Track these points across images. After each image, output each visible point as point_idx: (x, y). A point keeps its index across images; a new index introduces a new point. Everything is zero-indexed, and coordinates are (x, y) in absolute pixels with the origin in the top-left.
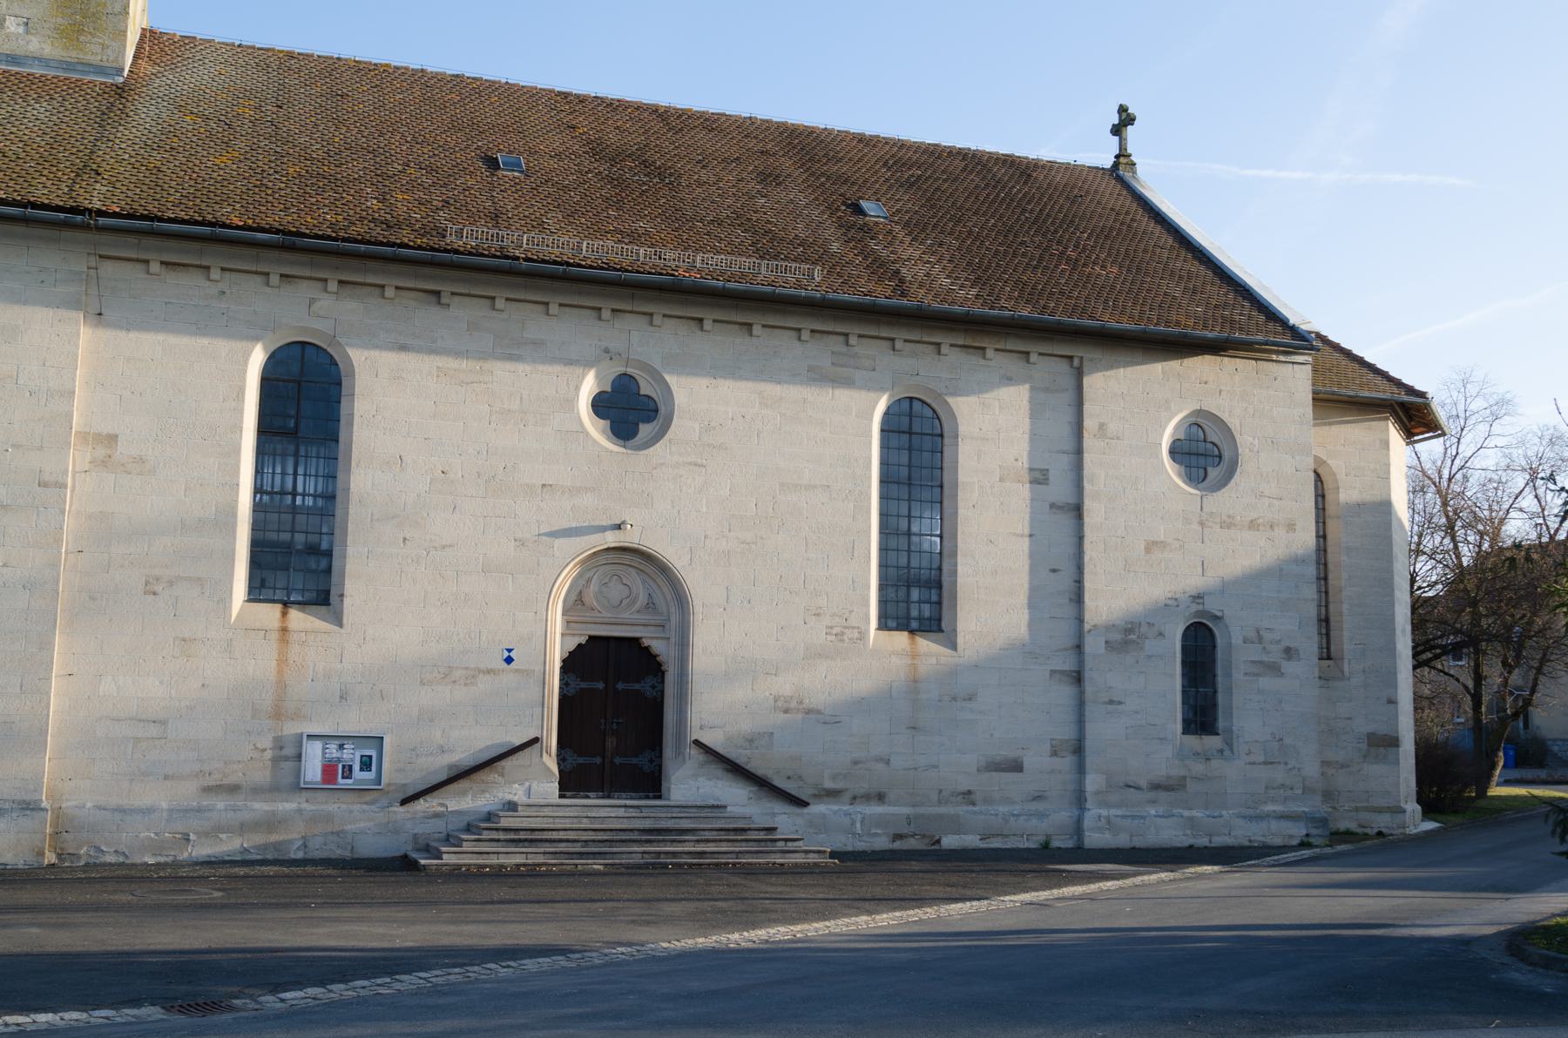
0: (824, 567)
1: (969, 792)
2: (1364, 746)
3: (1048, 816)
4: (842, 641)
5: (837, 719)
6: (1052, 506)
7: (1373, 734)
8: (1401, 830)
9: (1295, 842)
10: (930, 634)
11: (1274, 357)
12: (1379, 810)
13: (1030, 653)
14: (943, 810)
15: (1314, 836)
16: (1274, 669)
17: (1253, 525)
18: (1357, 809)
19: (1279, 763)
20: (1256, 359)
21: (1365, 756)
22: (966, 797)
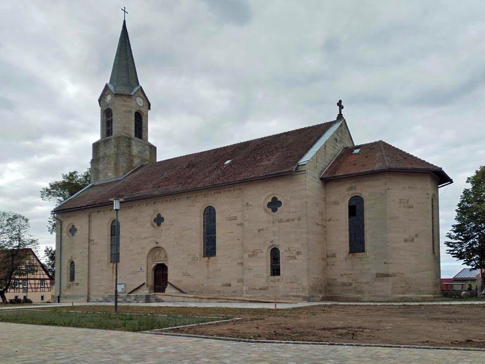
1: (219, 291)
6: (238, 225)
16: (294, 258)
17: (288, 221)
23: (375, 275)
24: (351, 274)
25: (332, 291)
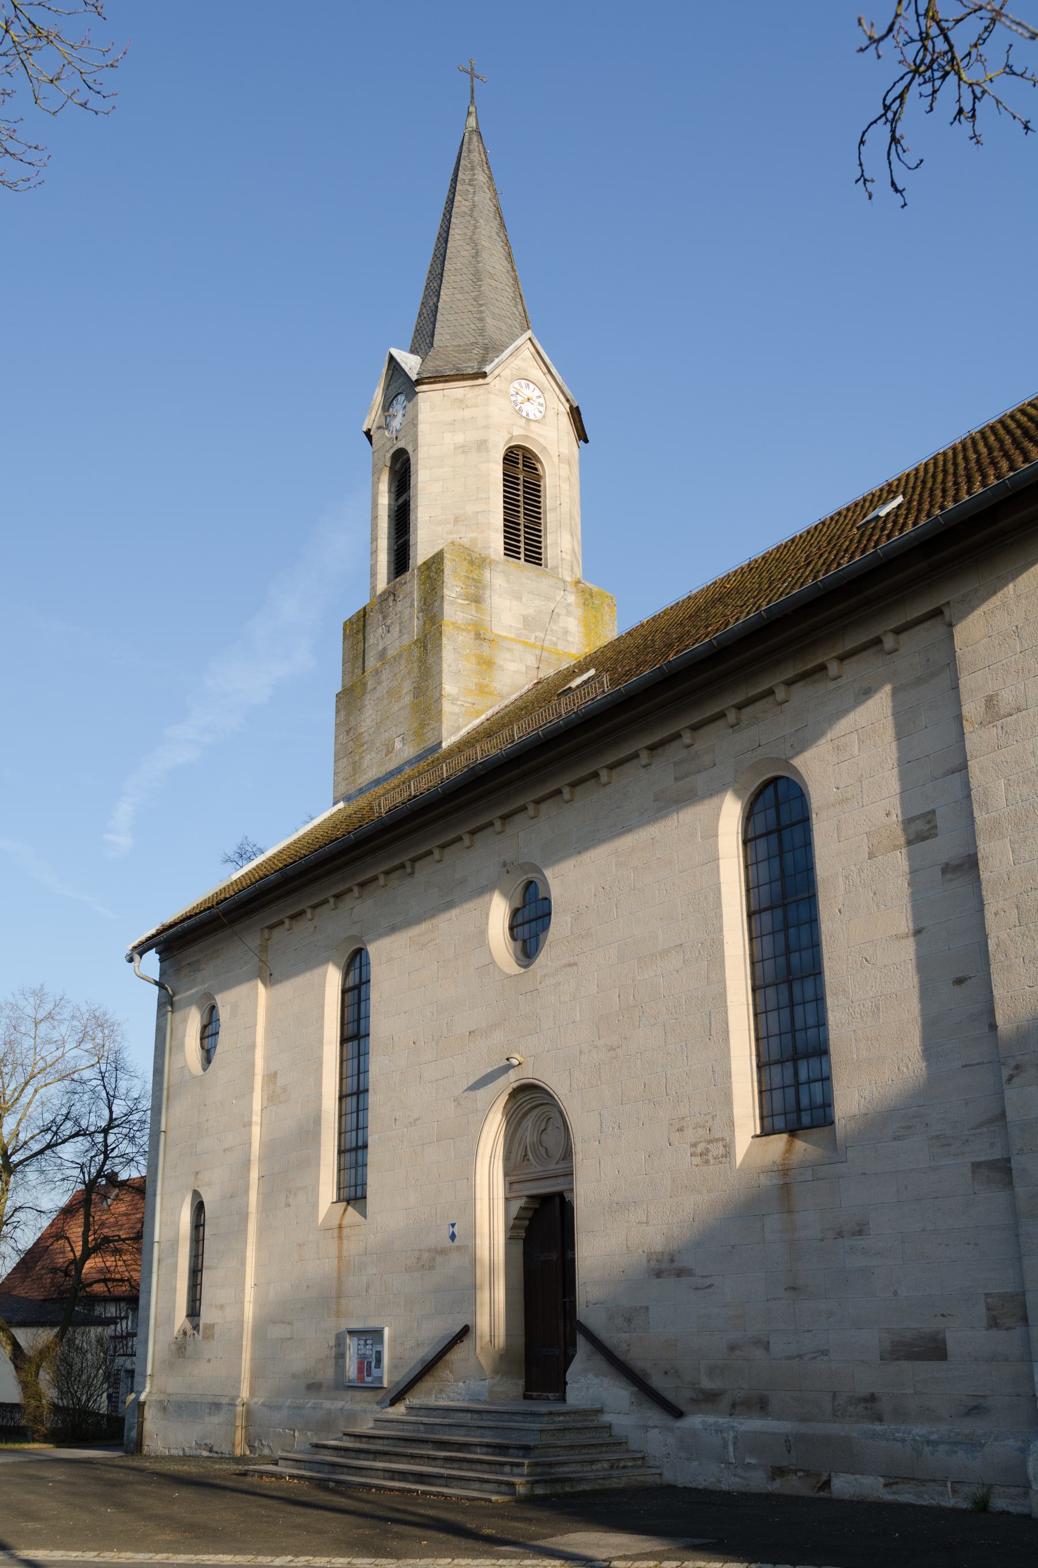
0: (683, 1059)
1: (872, 1398)
3: (982, 1446)
4: (707, 1162)
5: (708, 1281)
10: (814, 1130)
13: (938, 1137)
14: (836, 1429)
22: (869, 1406)
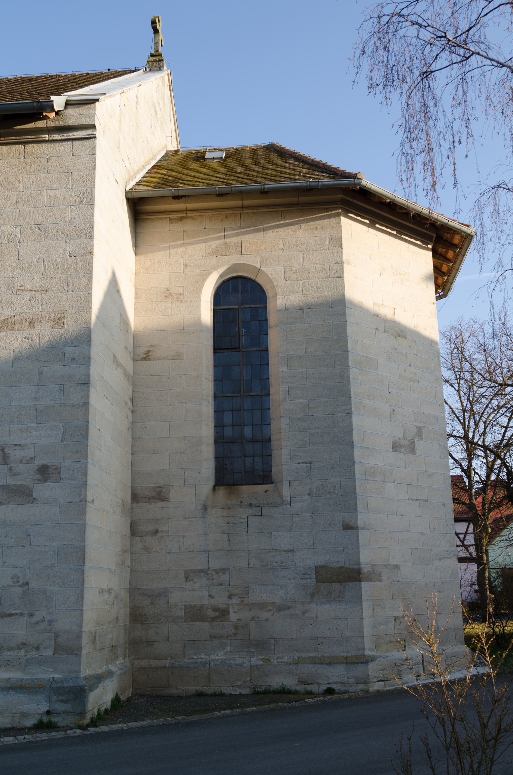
2: (312, 582)
7: (322, 567)
8: (361, 686)
9: (29, 722)
11: (46, 137)
12: (331, 662)
15: (58, 714)
18: (299, 662)
19: (22, 614)
20: (24, 143)
21: (312, 595)
23: (314, 576)
24: (224, 571)
25: (150, 643)
